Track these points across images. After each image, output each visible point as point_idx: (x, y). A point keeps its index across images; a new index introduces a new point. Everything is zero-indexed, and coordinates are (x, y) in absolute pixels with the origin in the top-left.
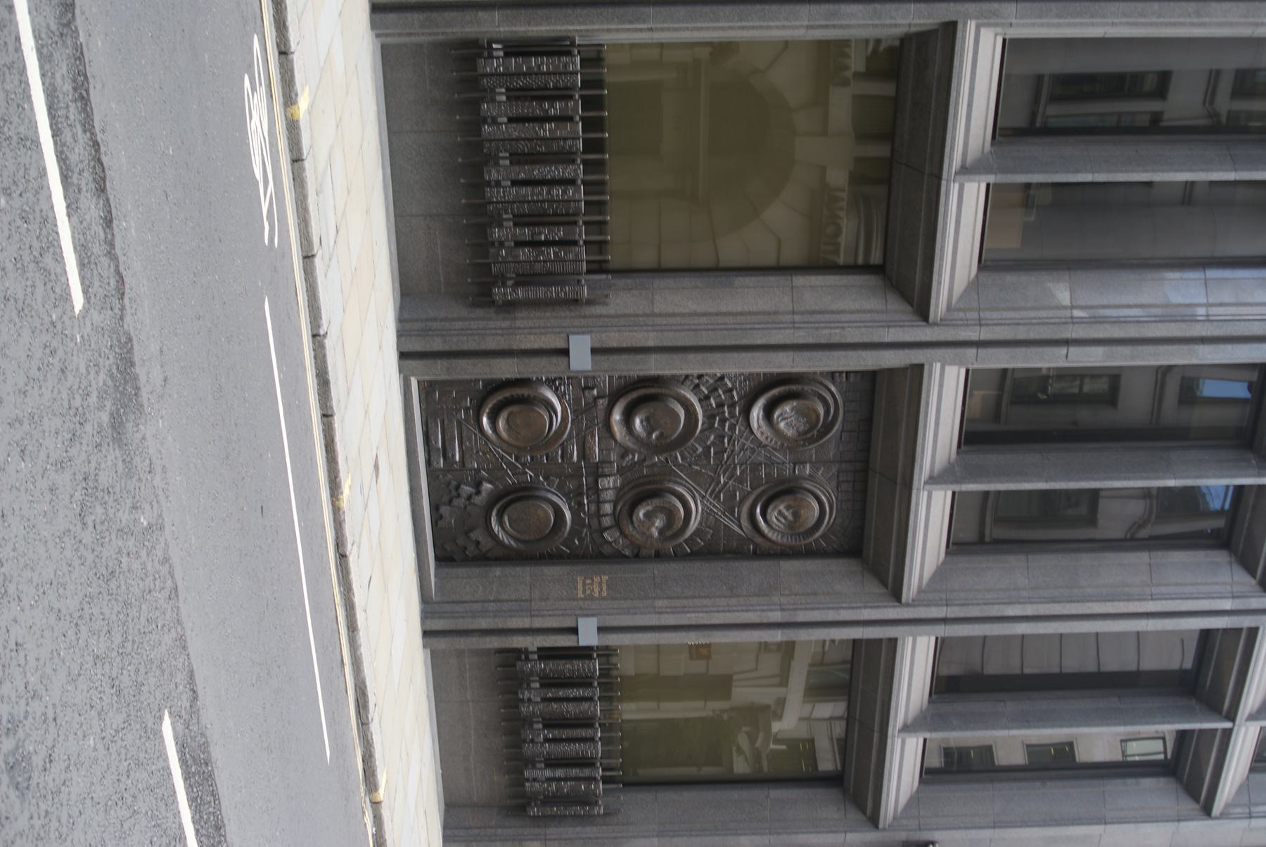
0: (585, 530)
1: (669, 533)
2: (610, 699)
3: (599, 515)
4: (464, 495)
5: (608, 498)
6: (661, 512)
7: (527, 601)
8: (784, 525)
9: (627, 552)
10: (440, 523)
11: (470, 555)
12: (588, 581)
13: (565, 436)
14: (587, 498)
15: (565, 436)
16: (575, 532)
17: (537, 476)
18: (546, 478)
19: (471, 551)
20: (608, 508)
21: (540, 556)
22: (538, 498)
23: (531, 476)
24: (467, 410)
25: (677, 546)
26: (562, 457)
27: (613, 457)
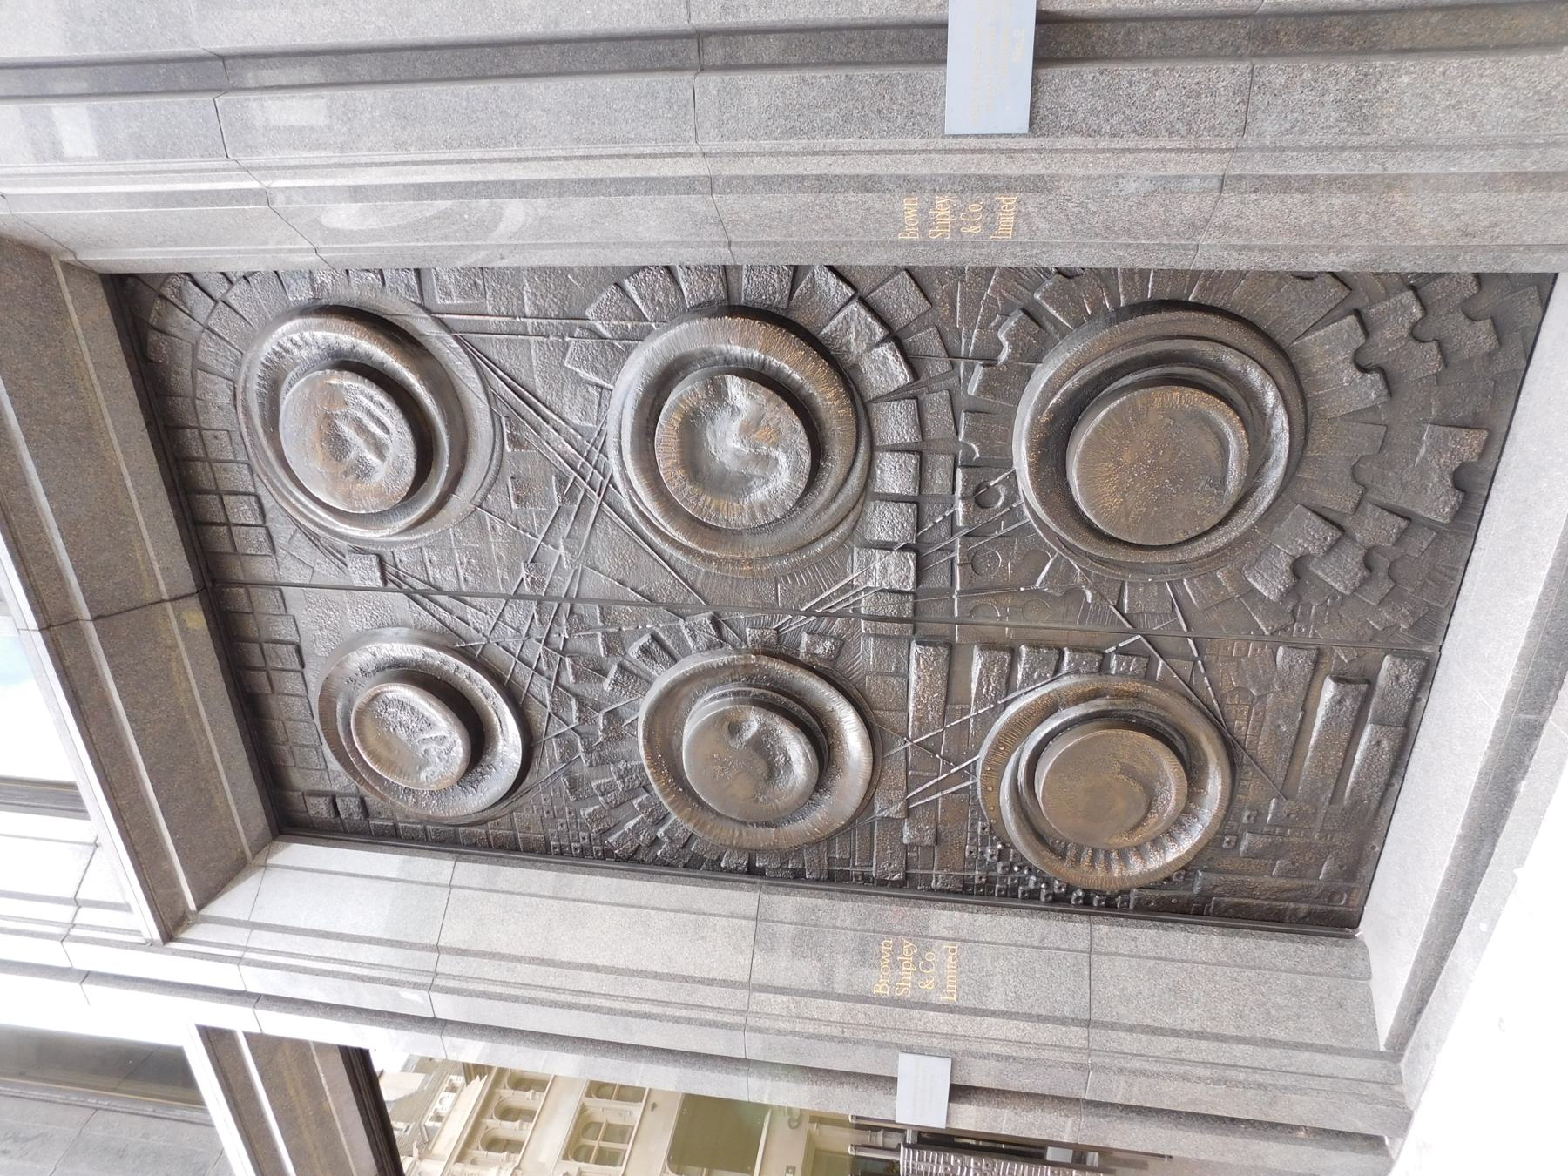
4: (1351, 558)
5: (890, 510)
14: (953, 515)
18: (1074, 593)
20: (893, 475)
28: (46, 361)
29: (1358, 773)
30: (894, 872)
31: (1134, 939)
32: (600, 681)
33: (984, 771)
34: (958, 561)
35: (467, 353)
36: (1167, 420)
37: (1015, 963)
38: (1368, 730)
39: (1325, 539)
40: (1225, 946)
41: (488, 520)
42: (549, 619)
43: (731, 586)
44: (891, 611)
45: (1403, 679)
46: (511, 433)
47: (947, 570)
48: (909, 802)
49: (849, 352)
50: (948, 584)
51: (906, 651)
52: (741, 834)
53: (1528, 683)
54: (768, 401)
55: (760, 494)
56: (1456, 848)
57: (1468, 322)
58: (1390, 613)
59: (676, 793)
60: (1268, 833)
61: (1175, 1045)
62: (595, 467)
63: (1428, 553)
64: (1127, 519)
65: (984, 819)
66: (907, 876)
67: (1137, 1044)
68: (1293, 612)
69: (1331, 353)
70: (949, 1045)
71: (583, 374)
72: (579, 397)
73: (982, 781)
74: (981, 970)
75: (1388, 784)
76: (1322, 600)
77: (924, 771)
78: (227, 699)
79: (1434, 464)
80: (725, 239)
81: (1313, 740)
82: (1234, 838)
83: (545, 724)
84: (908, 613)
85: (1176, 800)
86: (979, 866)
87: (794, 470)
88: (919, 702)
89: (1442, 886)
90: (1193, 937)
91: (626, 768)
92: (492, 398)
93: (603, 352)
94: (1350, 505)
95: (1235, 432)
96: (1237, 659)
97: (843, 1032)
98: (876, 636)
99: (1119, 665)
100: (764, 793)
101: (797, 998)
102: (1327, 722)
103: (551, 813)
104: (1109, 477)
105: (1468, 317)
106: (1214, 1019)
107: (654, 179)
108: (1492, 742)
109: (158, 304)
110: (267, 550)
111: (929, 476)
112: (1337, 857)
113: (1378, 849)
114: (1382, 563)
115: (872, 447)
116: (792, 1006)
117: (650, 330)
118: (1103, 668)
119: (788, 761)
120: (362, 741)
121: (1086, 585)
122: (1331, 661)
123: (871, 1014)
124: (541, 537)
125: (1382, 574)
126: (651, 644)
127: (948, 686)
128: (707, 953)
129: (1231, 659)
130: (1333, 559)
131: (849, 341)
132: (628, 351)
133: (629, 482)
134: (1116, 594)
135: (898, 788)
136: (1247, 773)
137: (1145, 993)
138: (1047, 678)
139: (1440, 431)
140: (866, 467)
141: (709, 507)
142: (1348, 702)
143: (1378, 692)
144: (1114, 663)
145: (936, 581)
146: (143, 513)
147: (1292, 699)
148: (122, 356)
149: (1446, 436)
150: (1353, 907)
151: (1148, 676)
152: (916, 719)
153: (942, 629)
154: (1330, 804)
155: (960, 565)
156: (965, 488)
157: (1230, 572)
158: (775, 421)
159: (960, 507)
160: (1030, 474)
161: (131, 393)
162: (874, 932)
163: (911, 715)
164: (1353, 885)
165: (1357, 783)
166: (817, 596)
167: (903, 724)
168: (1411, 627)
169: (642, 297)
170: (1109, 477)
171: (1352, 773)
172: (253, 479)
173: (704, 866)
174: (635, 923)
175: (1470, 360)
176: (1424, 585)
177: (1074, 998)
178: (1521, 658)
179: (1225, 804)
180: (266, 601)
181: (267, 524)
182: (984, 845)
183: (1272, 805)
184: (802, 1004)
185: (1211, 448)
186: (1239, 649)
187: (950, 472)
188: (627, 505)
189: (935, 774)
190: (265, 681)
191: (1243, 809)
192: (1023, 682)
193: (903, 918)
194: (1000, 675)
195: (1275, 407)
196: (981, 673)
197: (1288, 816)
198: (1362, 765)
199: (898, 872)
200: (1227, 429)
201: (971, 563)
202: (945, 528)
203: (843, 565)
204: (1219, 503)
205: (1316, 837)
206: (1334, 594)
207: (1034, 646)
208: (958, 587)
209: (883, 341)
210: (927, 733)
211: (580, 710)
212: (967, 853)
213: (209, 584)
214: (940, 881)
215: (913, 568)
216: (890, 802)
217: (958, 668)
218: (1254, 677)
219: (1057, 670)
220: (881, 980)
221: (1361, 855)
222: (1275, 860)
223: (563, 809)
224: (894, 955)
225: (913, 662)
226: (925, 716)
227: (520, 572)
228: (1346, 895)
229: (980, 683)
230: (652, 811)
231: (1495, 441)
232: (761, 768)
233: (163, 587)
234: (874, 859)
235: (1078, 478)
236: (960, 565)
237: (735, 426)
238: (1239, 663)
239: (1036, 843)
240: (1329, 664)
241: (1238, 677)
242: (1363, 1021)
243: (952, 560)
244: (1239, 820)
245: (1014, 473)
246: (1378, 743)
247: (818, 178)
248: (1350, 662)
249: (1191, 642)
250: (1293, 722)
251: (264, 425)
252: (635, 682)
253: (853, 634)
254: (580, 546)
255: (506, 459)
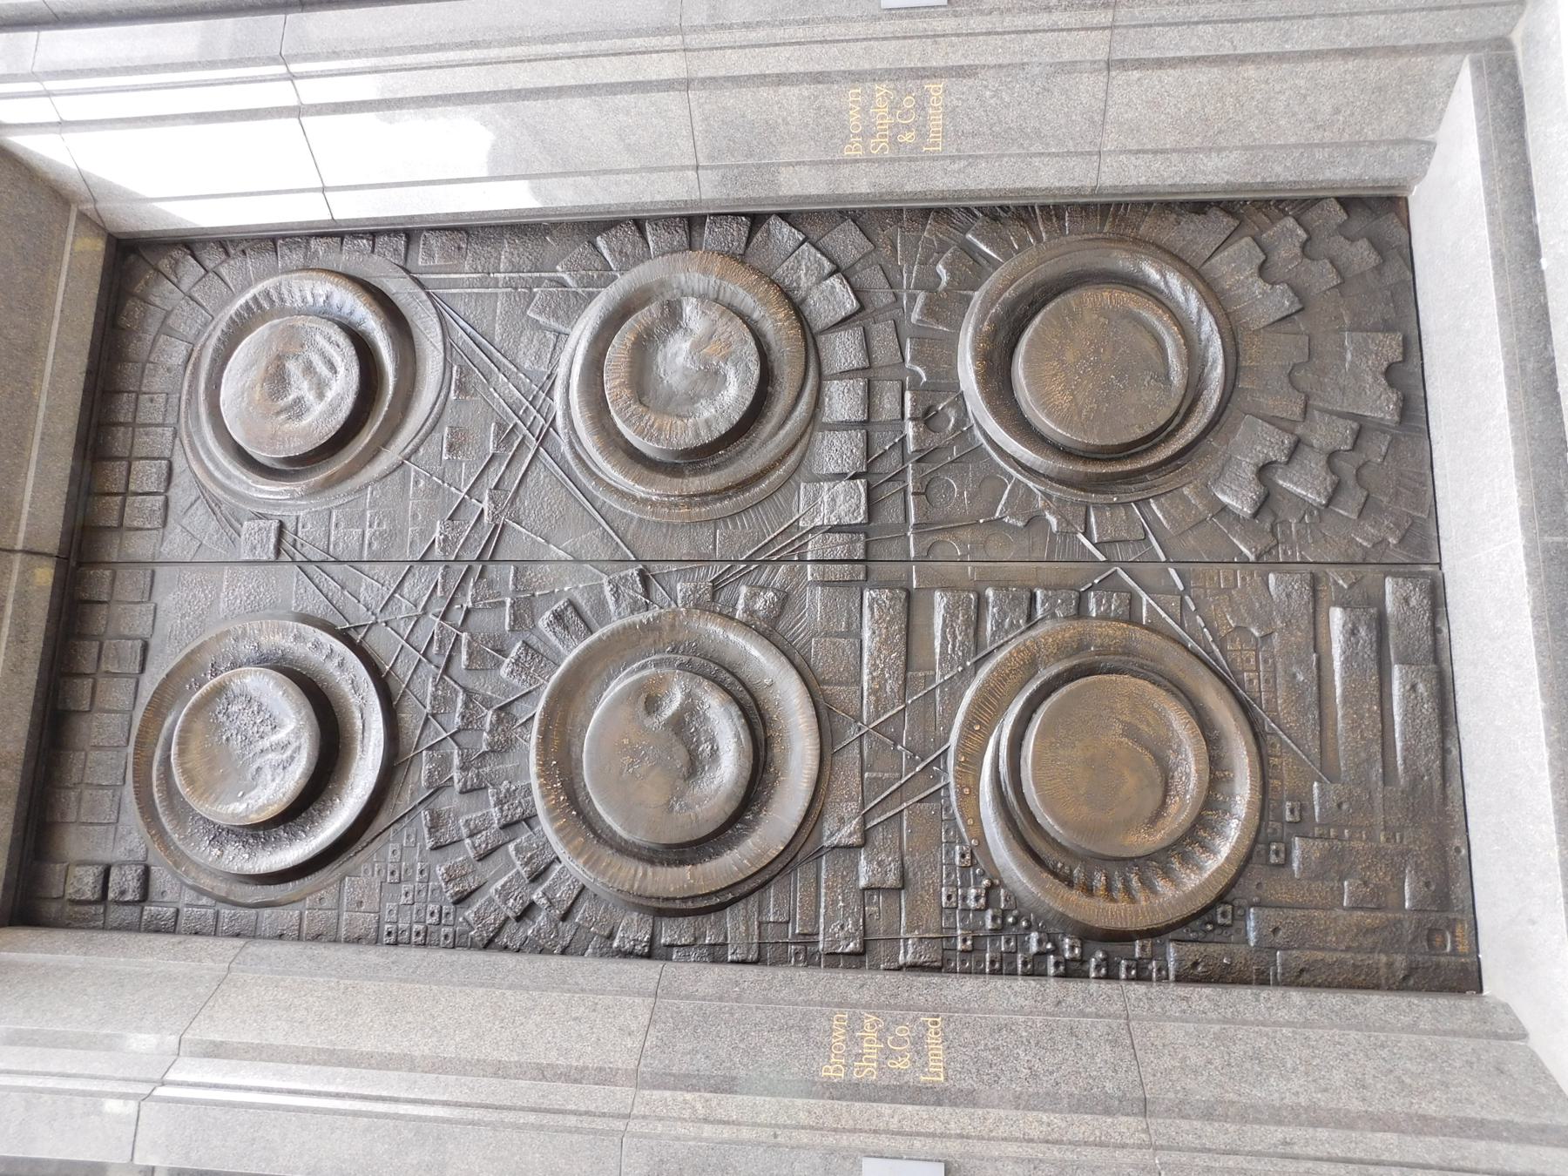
0: (915, 316)
1: (647, 315)
2: (1386, 907)
3: (868, 375)
4: (1314, 463)
5: (839, 440)
6: (671, 396)
7: (1123, 64)
8: (314, 344)
9: (785, 234)
10: (1390, 347)
11: (1290, 222)
12: (907, 138)
13: (969, 695)
14: (903, 440)
15: (969, 695)
16: (945, 307)
17: (1067, 534)
18: (1034, 520)
19: (1287, 235)
20: (842, 402)
21: (1061, 218)
22: (1065, 452)
23: (1087, 533)
24: (1301, 825)
25: (639, 260)
26: (981, 602)
27: (815, 601)
28: (20, 279)
29: (1403, 734)
30: (848, 938)
31: (1186, 999)
32: (498, 664)
33: (957, 763)
34: (911, 489)
35: (436, 307)
36: (1102, 319)
37: (1024, 1034)
38: (1396, 671)
39: (1283, 442)
40: (1311, 1005)
41: (413, 474)
42: (453, 584)
43: (665, 536)
44: (840, 553)
45: (1413, 602)
46: (460, 380)
47: (899, 502)
48: (864, 822)
49: (799, 288)
50: (901, 518)
51: (858, 601)
52: (645, 874)
53: (1538, 499)
54: (721, 316)
55: (706, 411)
56: (1547, 731)
57: (1348, 243)
58: (1374, 527)
59: (567, 816)
60: (1320, 837)
61: (1280, 1136)
62: (538, 411)
63: (1389, 458)
64: (1080, 416)
65: (962, 842)
66: (865, 943)
67: (1221, 1137)
68: (1273, 532)
69: (1239, 270)
70: (940, 1147)
71: (542, 319)
72: (535, 342)
73: (955, 777)
74: (976, 1044)
75: (1444, 751)
76: (1300, 516)
77: (883, 772)
78: (31, 698)
79: (1364, 366)
80: (694, 162)
81: (1338, 691)
82: (1282, 847)
83: (418, 732)
84: (859, 554)
85: (1197, 771)
86: (962, 920)
87: (744, 382)
88: (875, 666)
89: (1554, 793)
90: (1264, 994)
91: (508, 790)
92: (448, 347)
93: (567, 300)
94: (1298, 410)
95: (1168, 329)
96: (1227, 590)
97: (775, 1136)
98: (824, 583)
99: (1099, 604)
100: (681, 796)
101: (708, 1095)
102: (1347, 661)
103: (397, 875)
104: (1055, 375)
105: (1347, 238)
106: (1326, 1090)
107: (640, 82)
108: (1529, 574)
109: (151, 273)
110: (157, 523)
111: (877, 402)
112: (1417, 866)
113: (1464, 852)
114: (1347, 468)
115: (820, 376)
116: (699, 1106)
117: (616, 277)
118: (1080, 612)
119: (714, 753)
120: (182, 753)
121: (1049, 509)
122: (1329, 587)
123: (819, 1111)
124: (465, 490)
125: (1351, 482)
126: (566, 609)
127: (907, 645)
128: (580, 1035)
129: (1221, 592)
130: (1298, 467)
131: (799, 277)
132: (591, 296)
133: (572, 422)
134: (1082, 518)
135: (851, 799)
136: (1273, 745)
137: (1217, 1062)
138: (1019, 626)
139: (1358, 336)
140: (815, 393)
141: (652, 426)
142: (1363, 632)
143: (1392, 623)
144: (1092, 605)
145: (890, 514)
146: (41, 448)
147: (1300, 636)
148: (94, 304)
149: (1365, 340)
150: (1464, 955)
151: (1132, 618)
152: (873, 692)
153: (896, 570)
154: (1385, 784)
155: (914, 494)
156: (914, 407)
157: (1196, 487)
158: (726, 335)
159: (910, 429)
160: (978, 383)
161: (87, 337)
162: (821, 1004)
163: (865, 687)
164: (1451, 916)
165: (1406, 749)
166: (759, 542)
167: (856, 701)
168: (1401, 541)
169: (611, 250)
170: (1055, 375)
171: (1397, 735)
172: (173, 442)
173: (590, 950)
174: (481, 1005)
175: (1363, 274)
176: (1397, 494)
177: (1115, 1071)
178: (1518, 467)
179: (1258, 783)
180: (129, 585)
181: (169, 494)
182: (965, 885)
183: (1316, 792)
184: (714, 1104)
185: (1148, 345)
186: (1226, 579)
187: (898, 396)
188: (565, 448)
189: (897, 775)
190: (87, 692)
191: (1281, 803)
192: (993, 634)
193: (862, 986)
194: (967, 622)
195: (1200, 312)
196: (944, 621)
197: (1339, 805)
198: (1405, 723)
199: (854, 938)
200: (1160, 327)
201: (923, 492)
202: (896, 454)
203: (790, 505)
204: (1168, 397)
205: (1382, 838)
206: (1309, 508)
207: (1000, 586)
208: (913, 520)
209: (831, 274)
210: (885, 712)
211: (466, 705)
212: (944, 899)
213: (73, 563)
214: (911, 950)
215: (863, 495)
216: (842, 821)
217: (918, 620)
218: (1250, 610)
219: (1030, 616)
220: (833, 1060)
221: (1446, 863)
222: (1341, 880)
223: (413, 866)
224: (850, 1030)
225: (866, 611)
226: (882, 687)
227: (433, 533)
228: (1449, 937)
229: (944, 637)
230: (531, 858)
231: (1412, 346)
232: (680, 759)
233: (21, 536)
234: (822, 920)
235: (1026, 378)
236: (914, 494)
237: (686, 346)
238: (1231, 597)
239: (1031, 862)
240: (1328, 592)
241: (1234, 613)
242: (1543, 1090)
243: (905, 490)
244: (1280, 818)
245: (962, 394)
246: (1414, 687)
247: (778, 75)
248: (1351, 586)
249: (1172, 572)
250: (1309, 668)
251: (213, 360)
252: (540, 662)
253: (798, 584)
254: (506, 497)
255: (449, 404)
